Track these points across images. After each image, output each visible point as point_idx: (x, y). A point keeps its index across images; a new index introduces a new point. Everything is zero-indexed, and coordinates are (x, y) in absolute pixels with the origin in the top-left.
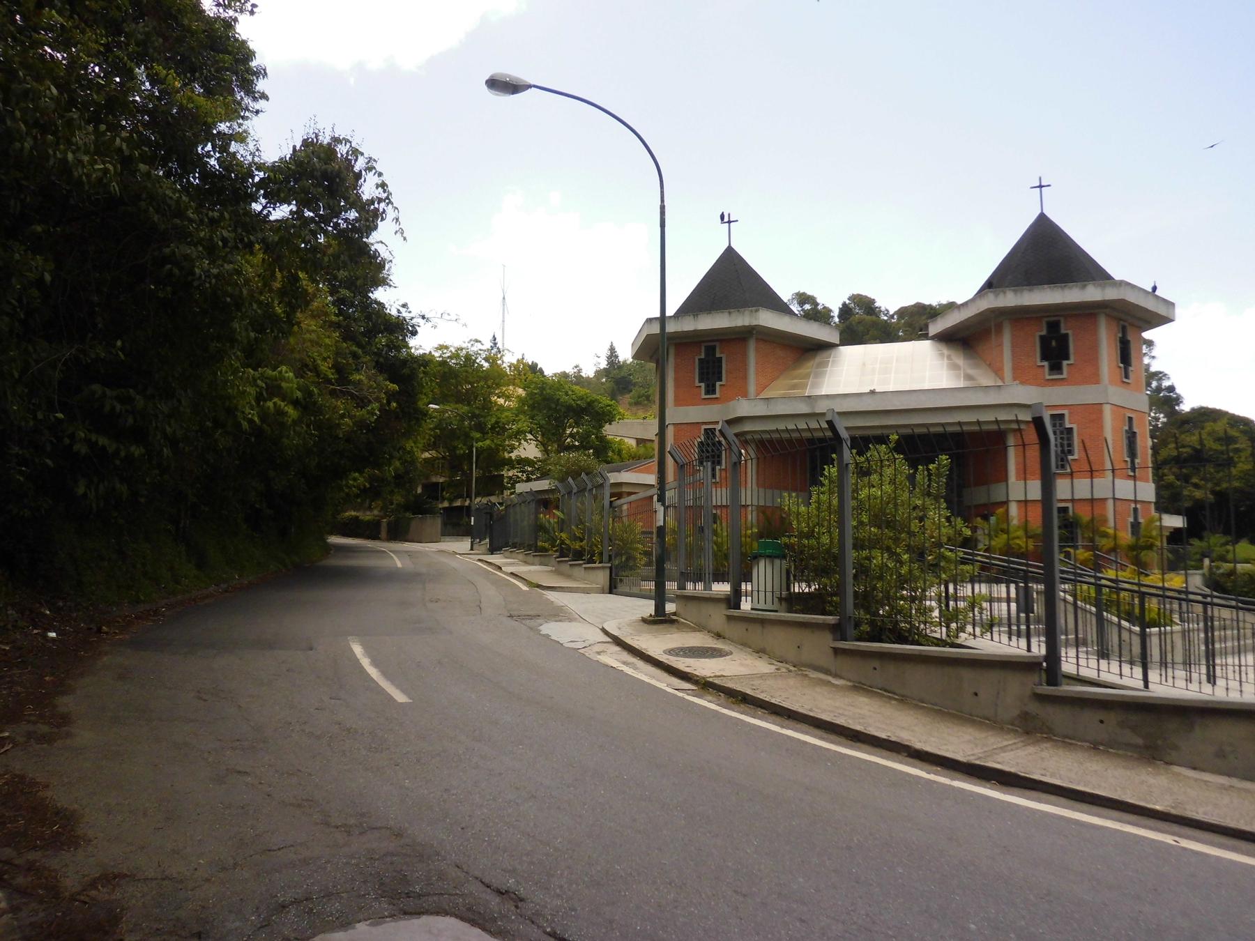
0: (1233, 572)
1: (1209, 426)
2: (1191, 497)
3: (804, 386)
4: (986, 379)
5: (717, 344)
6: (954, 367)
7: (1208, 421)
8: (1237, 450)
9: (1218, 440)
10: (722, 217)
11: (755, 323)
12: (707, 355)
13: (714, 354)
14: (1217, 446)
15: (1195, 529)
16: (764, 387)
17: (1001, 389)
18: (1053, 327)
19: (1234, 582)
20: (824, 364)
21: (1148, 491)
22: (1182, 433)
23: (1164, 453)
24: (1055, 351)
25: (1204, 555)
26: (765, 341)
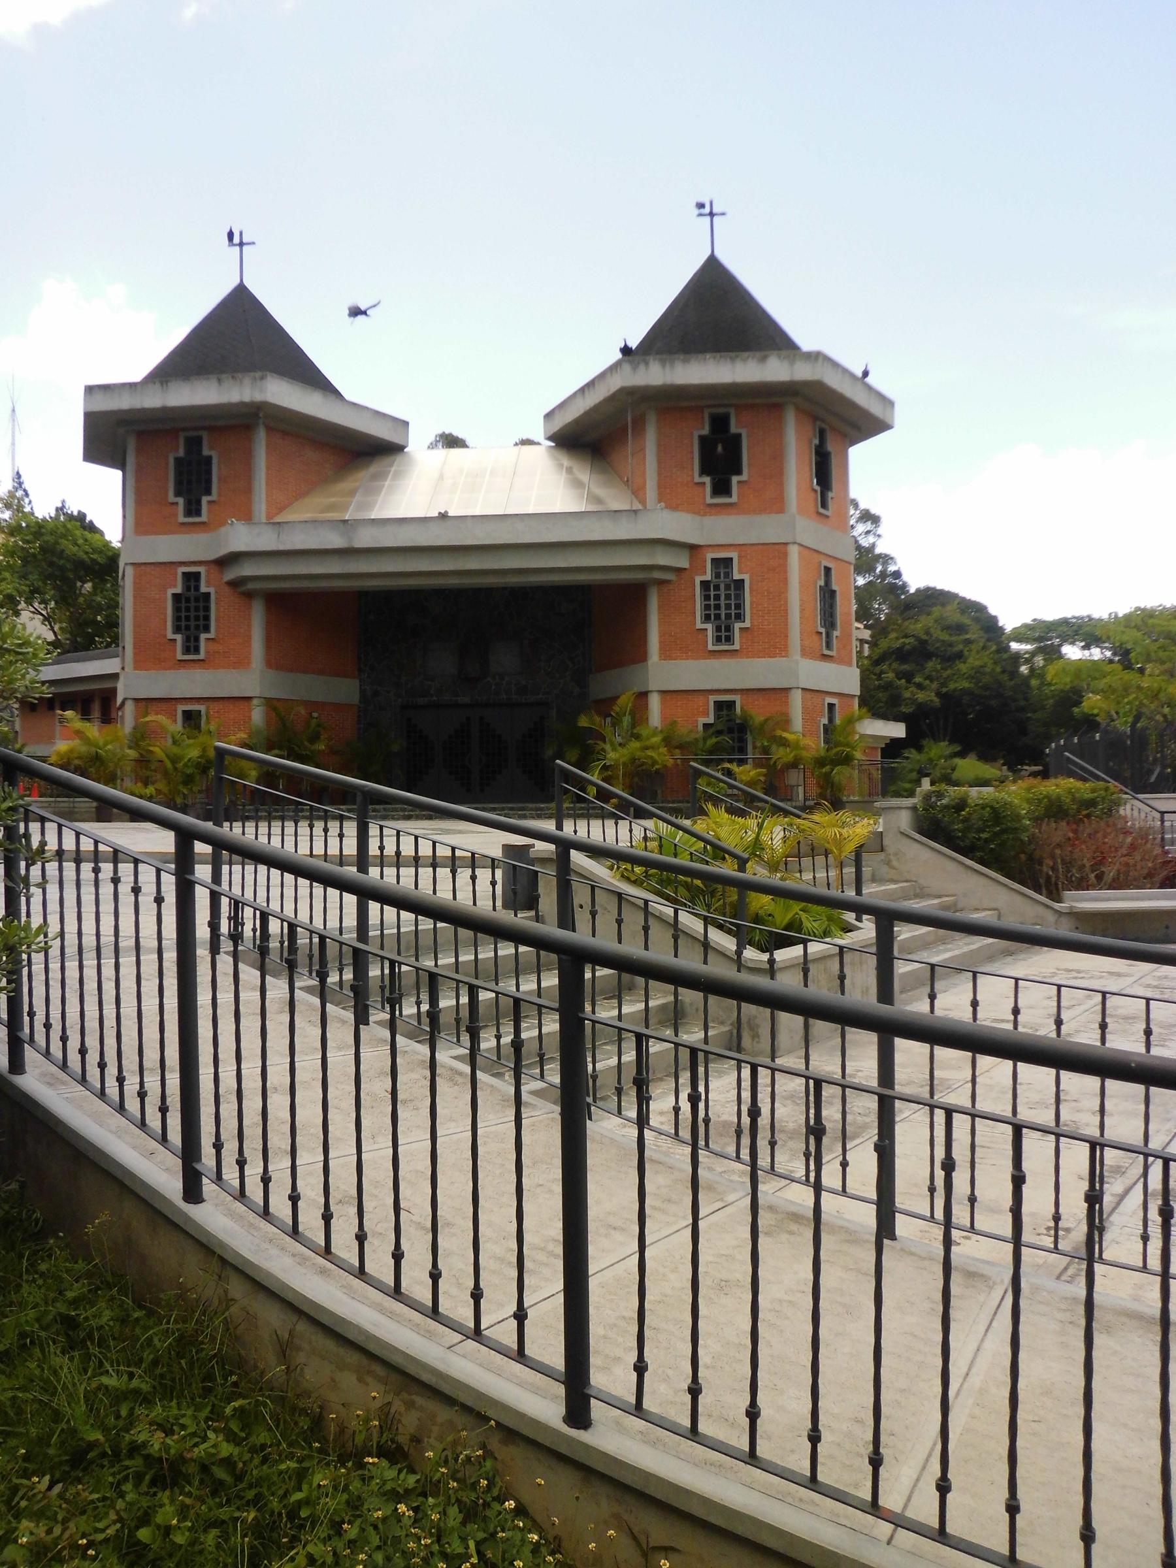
0: (961, 804)
1: (936, 611)
2: (914, 701)
3: (345, 508)
4: (617, 501)
5: (205, 435)
6: (577, 484)
7: (934, 604)
8: (968, 642)
9: (947, 628)
10: (231, 235)
11: (258, 397)
12: (188, 451)
13: (200, 451)
14: (945, 636)
15: (913, 740)
16: (281, 509)
17: (646, 517)
18: (720, 423)
19: (966, 820)
20: (381, 476)
21: (846, 679)
22: (904, 620)
23: (884, 644)
24: (721, 462)
25: (923, 774)
26: (285, 434)
